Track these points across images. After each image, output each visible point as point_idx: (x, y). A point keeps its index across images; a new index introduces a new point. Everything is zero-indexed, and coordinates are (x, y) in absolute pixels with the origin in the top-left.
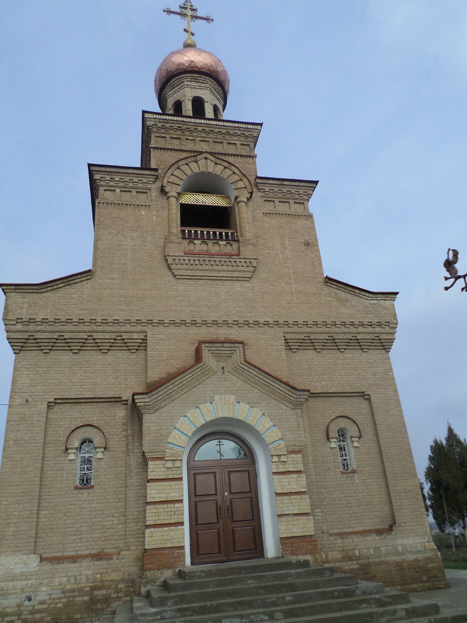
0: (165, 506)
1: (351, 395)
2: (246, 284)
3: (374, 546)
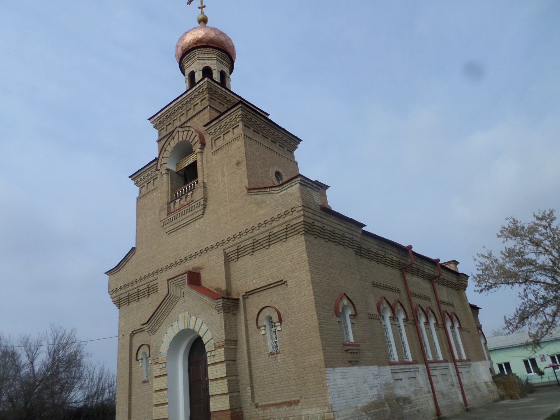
0: (159, 393)
1: (275, 285)
2: (202, 220)
3: (285, 416)
